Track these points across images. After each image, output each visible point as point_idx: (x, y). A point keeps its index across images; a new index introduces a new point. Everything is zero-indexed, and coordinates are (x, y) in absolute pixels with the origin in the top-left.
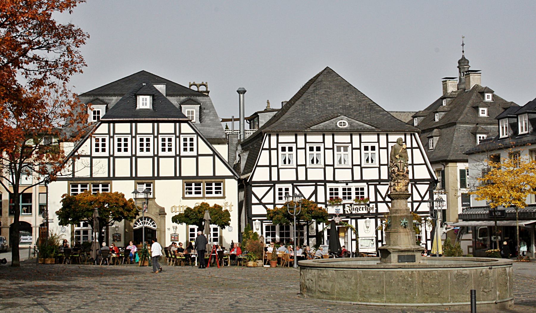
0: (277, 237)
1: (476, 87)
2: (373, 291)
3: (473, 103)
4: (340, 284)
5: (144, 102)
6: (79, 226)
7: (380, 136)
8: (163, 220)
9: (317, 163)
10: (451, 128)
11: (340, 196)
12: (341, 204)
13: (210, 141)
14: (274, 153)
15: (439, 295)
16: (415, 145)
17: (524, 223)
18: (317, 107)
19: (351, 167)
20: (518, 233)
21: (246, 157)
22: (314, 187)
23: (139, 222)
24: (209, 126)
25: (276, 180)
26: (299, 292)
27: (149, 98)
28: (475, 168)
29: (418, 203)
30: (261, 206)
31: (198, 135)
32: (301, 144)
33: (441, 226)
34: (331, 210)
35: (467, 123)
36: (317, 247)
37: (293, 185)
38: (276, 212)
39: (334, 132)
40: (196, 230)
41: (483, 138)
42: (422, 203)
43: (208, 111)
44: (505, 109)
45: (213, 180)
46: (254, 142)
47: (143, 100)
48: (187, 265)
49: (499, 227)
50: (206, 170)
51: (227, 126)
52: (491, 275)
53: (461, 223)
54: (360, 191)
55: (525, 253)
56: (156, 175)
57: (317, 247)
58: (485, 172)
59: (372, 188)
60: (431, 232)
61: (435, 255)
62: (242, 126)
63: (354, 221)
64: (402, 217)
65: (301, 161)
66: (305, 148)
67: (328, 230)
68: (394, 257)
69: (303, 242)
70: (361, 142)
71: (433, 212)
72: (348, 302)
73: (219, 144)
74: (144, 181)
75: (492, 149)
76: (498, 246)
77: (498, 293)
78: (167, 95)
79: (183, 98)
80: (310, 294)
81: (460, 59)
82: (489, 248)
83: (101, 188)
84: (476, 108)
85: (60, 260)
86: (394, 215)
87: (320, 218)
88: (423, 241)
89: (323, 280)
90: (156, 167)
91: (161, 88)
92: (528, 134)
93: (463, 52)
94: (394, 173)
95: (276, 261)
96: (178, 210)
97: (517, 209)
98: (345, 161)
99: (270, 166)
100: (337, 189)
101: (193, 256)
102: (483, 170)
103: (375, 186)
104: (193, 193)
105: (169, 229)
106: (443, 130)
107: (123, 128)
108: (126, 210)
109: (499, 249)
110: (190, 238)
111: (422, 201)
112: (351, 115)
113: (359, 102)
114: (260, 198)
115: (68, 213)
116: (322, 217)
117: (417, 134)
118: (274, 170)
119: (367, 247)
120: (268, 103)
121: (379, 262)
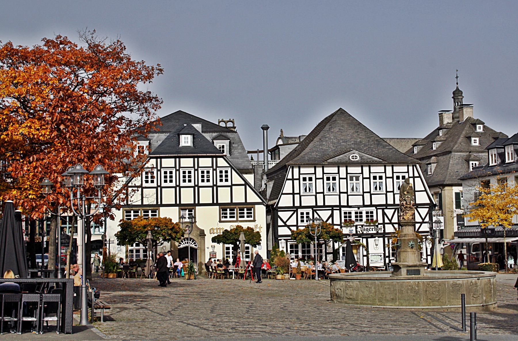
0: (300, 254)
1: (469, 119)
2: (388, 297)
3: (466, 133)
4: (363, 292)
5: (186, 141)
6: (132, 246)
7: (387, 168)
8: (203, 240)
9: (333, 190)
10: (446, 156)
11: (353, 218)
12: (353, 226)
13: (241, 172)
14: (296, 182)
15: (439, 300)
16: (416, 174)
17: (510, 240)
18: (333, 143)
19: (362, 194)
20: (505, 249)
21: (272, 186)
22: (330, 212)
23: (182, 242)
24: (238, 158)
25: (299, 205)
26: (330, 299)
27: (190, 137)
28: (469, 191)
29: (419, 224)
30: (286, 228)
31: (232, 168)
32: (319, 174)
33: (439, 243)
34: (345, 231)
35: (461, 151)
36: (333, 262)
37: (312, 209)
38: (299, 233)
39: (347, 164)
40: (231, 249)
41: (475, 164)
42: (423, 224)
43: (237, 145)
44: (496, 139)
45: (245, 206)
46: (279, 172)
47: (185, 139)
48: (226, 278)
49: (490, 244)
50: (239, 198)
51: (252, 157)
52: (479, 284)
53: (457, 240)
54: (369, 214)
55: (513, 266)
56: (197, 202)
57: (333, 262)
58: (477, 196)
59: (380, 212)
60: (431, 249)
61: (434, 269)
62: (266, 158)
63: (365, 240)
64: (409, 240)
65: (320, 190)
66: (323, 178)
67: (343, 248)
68: (404, 271)
69: (322, 258)
70: (370, 172)
71: (432, 232)
72: (369, 306)
73: (246, 173)
74: (186, 207)
75: (482, 176)
76: (489, 260)
77: (484, 298)
78: (202, 132)
79: (215, 134)
80: (339, 300)
81: (455, 90)
82: (481, 261)
83: (150, 213)
84: (469, 138)
85: (119, 275)
86: (403, 238)
87: (337, 238)
88: (424, 256)
89: (350, 289)
90: (197, 195)
91: (198, 127)
92: (514, 162)
93: (457, 83)
94: (403, 206)
95: (301, 275)
96: (215, 231)
97: (504, 228)
98: (357, 188)
99: (293, 194)
100: (350, 213)
101: (230, 271)
102: (476, 193)
103: (383, 209)
104: (228, 217)
105: (208, 248)
106: (440, 157)
107: (168, 163)
108: (174, 232)
109: (489, 262)
110: (226, 255)
111: (423, 222)
112: (361, 149)
113: (368, 138)
114: (285, 221)
115: (125, 235)
116: (338, 237)
117: (418, 165)
118: (297, 197)
119: (376, 262)
120: (282, 131)
121: (391, 275)
